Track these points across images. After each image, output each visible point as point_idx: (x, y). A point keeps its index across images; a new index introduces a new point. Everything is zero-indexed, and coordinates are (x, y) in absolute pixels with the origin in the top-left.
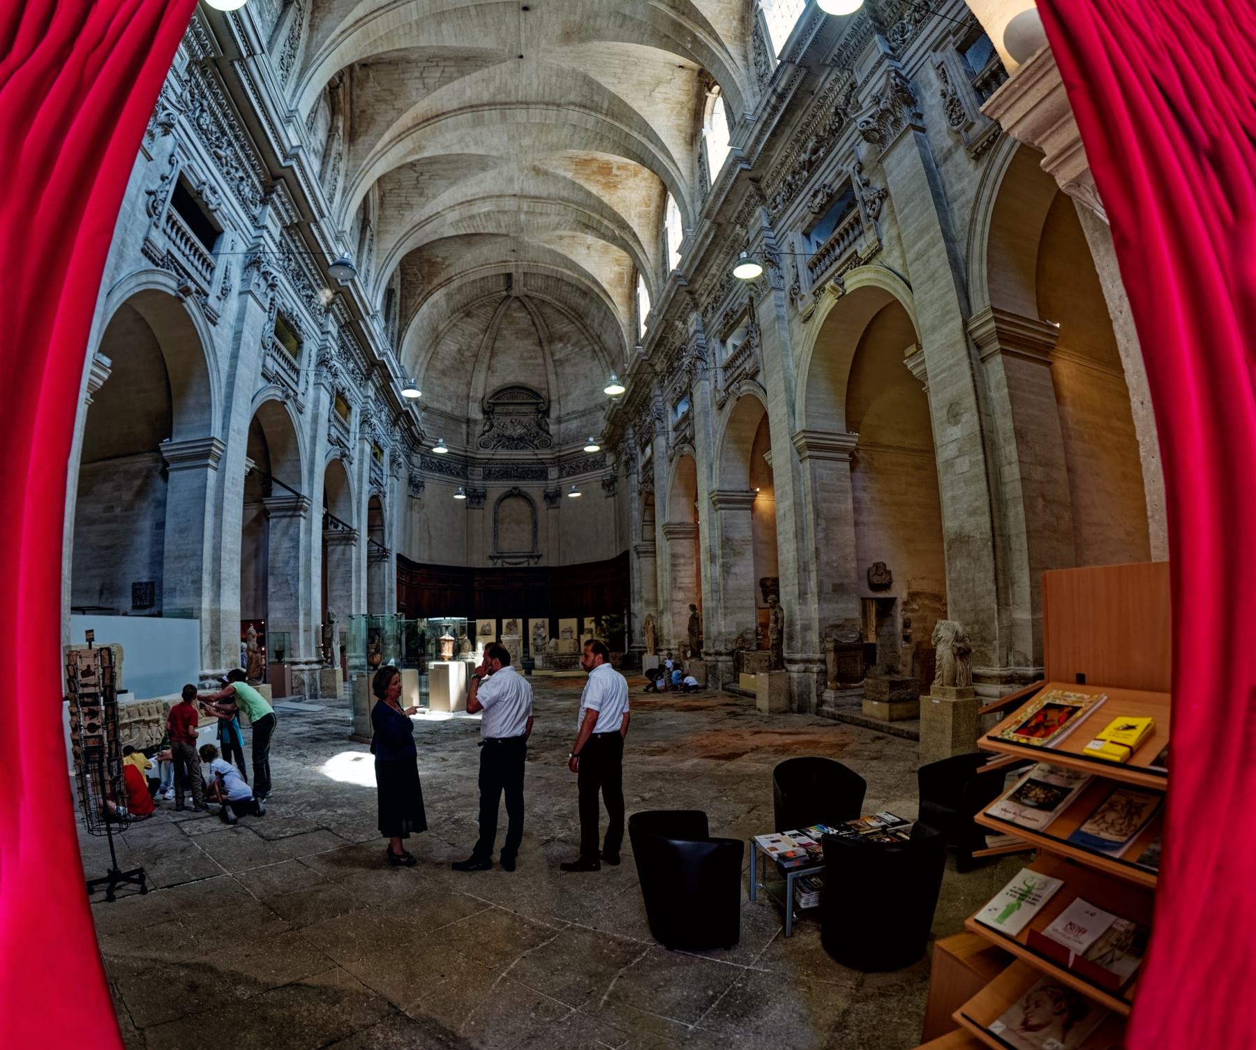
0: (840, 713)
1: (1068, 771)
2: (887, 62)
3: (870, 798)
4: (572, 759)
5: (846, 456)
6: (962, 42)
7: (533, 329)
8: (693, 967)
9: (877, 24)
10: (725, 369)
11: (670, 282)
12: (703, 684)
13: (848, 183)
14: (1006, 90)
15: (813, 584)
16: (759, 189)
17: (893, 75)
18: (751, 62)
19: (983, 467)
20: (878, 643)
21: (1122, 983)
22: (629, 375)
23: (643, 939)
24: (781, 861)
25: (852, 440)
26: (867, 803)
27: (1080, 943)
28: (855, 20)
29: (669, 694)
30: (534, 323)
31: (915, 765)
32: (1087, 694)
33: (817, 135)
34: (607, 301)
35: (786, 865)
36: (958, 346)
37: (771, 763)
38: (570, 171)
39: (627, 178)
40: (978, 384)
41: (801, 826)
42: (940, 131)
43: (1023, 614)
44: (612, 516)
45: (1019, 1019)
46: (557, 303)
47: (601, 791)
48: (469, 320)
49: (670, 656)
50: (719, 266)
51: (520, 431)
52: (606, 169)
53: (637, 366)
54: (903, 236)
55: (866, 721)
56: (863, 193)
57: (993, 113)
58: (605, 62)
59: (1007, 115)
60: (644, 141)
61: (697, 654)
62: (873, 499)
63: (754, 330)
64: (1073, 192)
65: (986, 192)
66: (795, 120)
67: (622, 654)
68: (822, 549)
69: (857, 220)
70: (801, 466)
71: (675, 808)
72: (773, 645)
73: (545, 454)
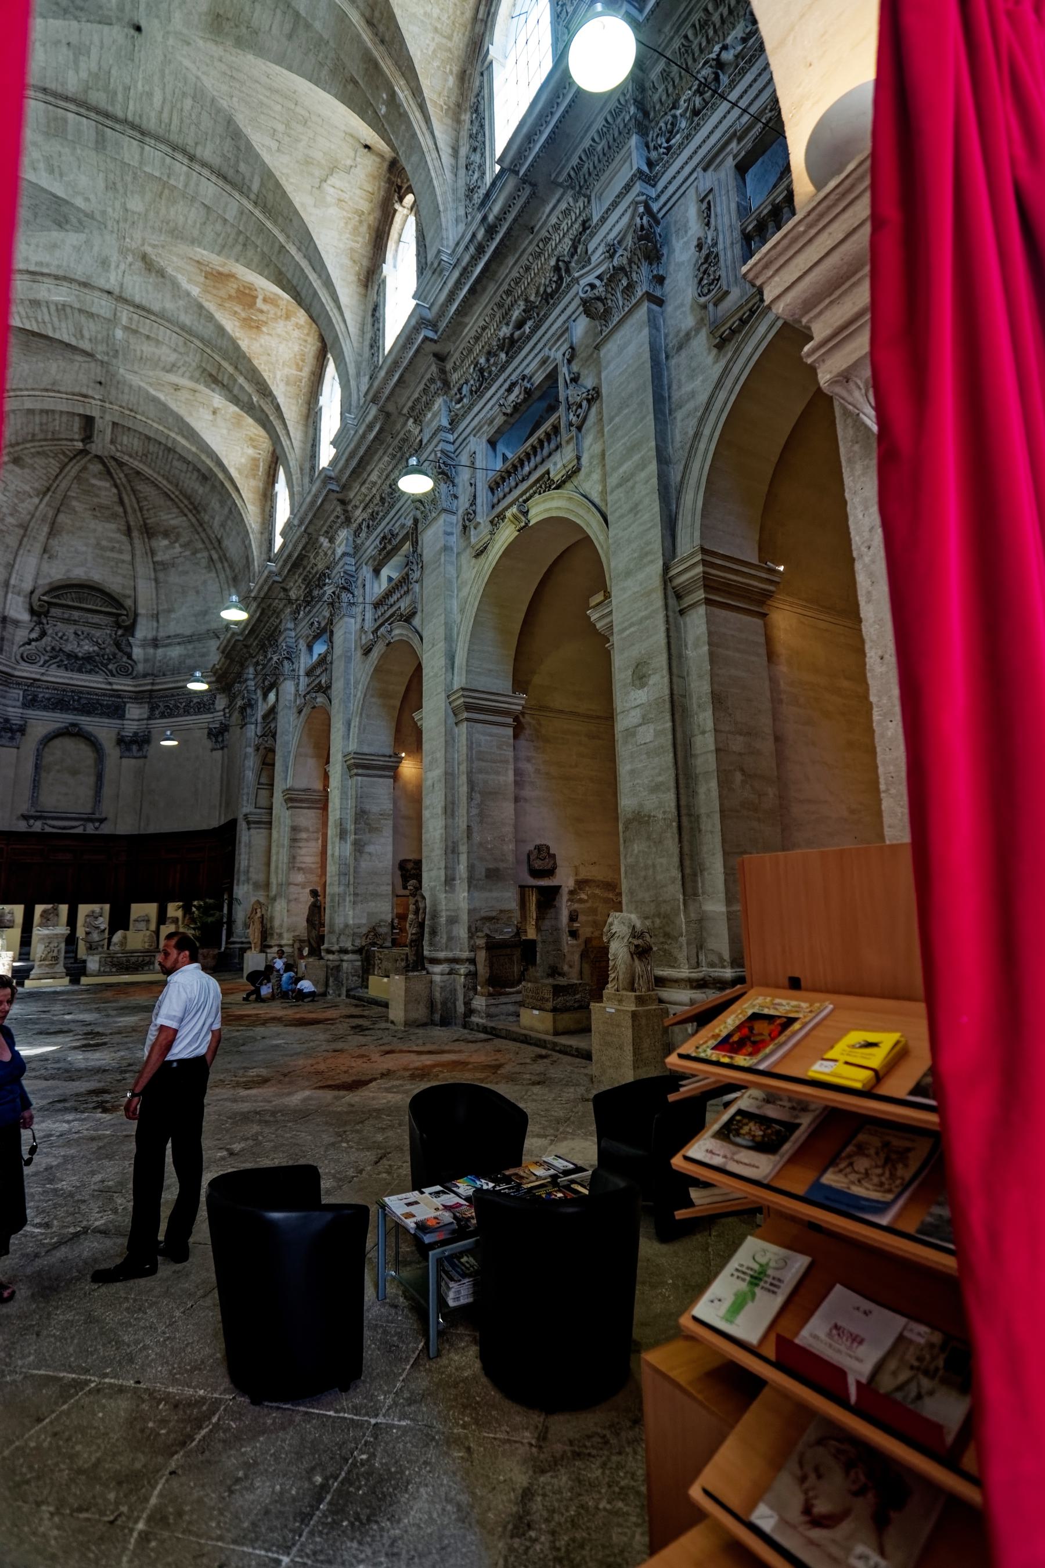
0: (492, 1024)
1: (790, 1100)
2: (638, 187)
3: (533, 1136)
4: (130, 1101)
5: (510, 720)
6: (747, 153)
7: (120, 510)
8: (291, 1431)
9: (640, 115)
10: (376, 605)
11: (318, 484)
12: (321, 990)
13: (552, 377)
14: (785, 236)
15: (462, 869)
16: (443, 371)
17: (641, 209)
18: (462, 161)
19: (670, 737)
20: (539, 939)
21: (950, 1439)
22: (255, 598)
23: (215, 1390)
24: (420, 1234)
25: (518, 702)
26: (530, 1143)
27: (859, 1360)
28: (612, 105)
29: (277, 1003)
30: (121, 502)
31: (588, 1090)
32: (805, 1001)
33: (526, 300)
34: (234, 495)
35: (428, 1239)
36: (654, 596)
37: (406, 1092)
38: (196, 284)
39: (276, 319)
40: (672, 641)
41: (445, 1180)
42: (682, 305)
43: (715, 906)
44: (217, 775)
45: (796, 1503)
46: (165, 482)
47: (169, 1145)
48: (17, 469)
49: (281, 954)
50: (382, 471)
51: (87, 647)
52: (246, 297)
53: (266, 588)
54: (607, 454)
55: (525, 1035)
56: (569, 392)
57: (756, 277)
58: (262, 103)
59: (776, 279)
60: (304, 264)
61: (315, 952)
62: (538, 771)
63: (415, 561)
64: (838, 389)
65: (722, 396)
66: (503, 271)
67: (216, 951)
68: (475, 828)
69: (556, 429)
70: (456, 730)
71: (276, 1163)
72: (412, 941)
73: (123, 684)
